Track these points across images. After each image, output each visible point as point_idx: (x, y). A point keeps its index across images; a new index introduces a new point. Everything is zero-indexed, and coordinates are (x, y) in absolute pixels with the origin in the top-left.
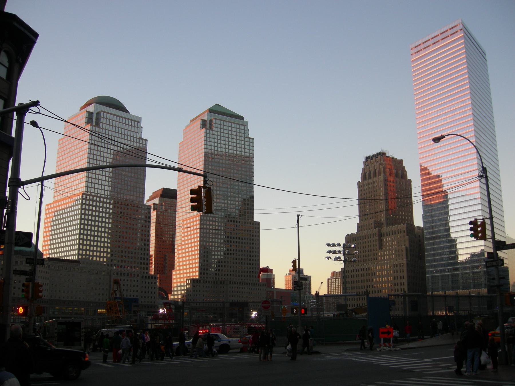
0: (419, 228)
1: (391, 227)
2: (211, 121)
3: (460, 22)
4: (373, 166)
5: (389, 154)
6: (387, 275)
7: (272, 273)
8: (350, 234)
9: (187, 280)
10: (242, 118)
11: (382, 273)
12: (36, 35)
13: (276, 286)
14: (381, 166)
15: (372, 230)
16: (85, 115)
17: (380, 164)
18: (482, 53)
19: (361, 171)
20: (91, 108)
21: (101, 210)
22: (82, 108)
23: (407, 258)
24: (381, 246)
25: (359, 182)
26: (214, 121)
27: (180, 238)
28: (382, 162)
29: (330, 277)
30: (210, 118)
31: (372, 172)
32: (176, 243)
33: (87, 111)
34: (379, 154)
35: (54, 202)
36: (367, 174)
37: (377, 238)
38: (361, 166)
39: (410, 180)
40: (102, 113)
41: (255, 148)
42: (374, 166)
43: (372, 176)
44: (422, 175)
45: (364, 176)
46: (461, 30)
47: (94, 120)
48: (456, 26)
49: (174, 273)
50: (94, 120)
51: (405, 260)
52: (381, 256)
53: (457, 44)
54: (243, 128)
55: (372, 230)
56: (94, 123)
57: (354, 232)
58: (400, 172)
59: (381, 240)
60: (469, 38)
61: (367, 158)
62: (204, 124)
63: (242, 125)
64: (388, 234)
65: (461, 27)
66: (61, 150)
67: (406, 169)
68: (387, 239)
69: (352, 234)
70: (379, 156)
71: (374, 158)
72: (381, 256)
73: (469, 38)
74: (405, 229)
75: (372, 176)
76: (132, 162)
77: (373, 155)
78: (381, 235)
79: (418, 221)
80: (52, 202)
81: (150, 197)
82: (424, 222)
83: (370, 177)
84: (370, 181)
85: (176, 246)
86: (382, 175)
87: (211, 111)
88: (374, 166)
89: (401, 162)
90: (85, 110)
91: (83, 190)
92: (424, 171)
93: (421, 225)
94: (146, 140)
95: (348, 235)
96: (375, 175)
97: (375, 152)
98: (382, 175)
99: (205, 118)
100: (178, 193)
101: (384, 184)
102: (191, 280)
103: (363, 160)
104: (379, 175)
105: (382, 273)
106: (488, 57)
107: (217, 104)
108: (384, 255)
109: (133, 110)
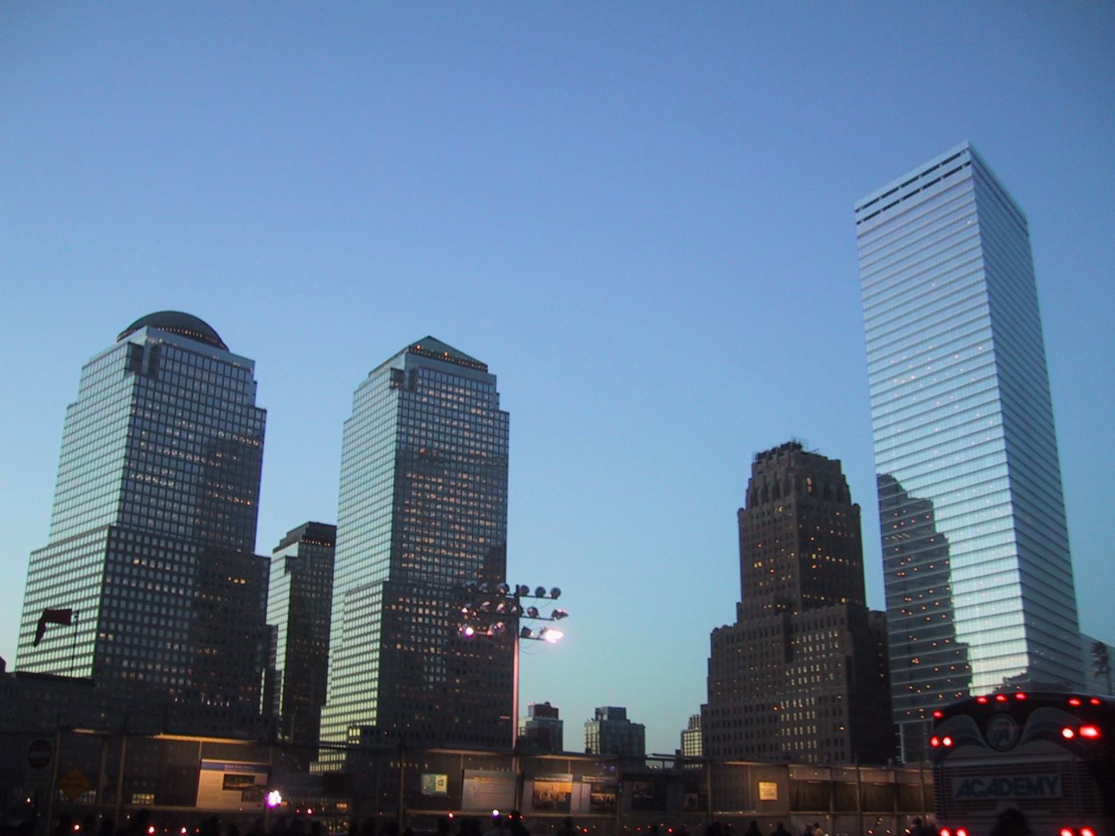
0: (878, 614)
1: (812, 610)
2: (413, 372)
3: (967, 146)
4: (772, 473)
5: (809, 448)
6: (805, 723)
7: (557, 716)
8: (720, 627)
9: (349, 728)
10: (483, 367)
11: (792, 717)
12: (254, 362)
13: (567, 747)
14: (791, 475)
15: (769, 618)
16: (124, 351)
17: (789, 469)
18: (1018, 222)
19: (746, 486)
20: (140, 338)
21: (152, 565)
22: (122, 336)
23: (849, 682)
24: (790, 655)
25: (741, 510)
26: (420, 372)
27: (340, 633)
28: (793, 464)
29: (686, 728)
30: (411, 366)
31: (770, 488)
32: (332, 644)
33: (129, 343)
34: (784, 447)
35: (50, 546)
36: (759, 492)
37: (781, 636)
38: (745, 474)
39: (856, 505)
40: (164, 348)
41: (511, 435)
42: (775, 475)
43: (770, 495)
44: (881, 492)
45: (754, 495)
46: (968, 164)
47: (145, 363)
48: (958, 155)
49: (324, 712)
50: (145, 363)
51: (844, 686)
52: (810, 708)
53: (961, 198)
54: (486, 388)
55: (769, 618)
56: (145, 370)
57: (730, 624)
58: (833, 488)
59: (788, 640)
60: (989, 189)
61: (760, 456)
62: (397, 376)
63: (483, 383)
64: (807, 628)
65: (966, 158)
66: (71, 430)
67: (848, 481)
68: (806, 642)
69: (725, 627)
70: (786, 452)
71: (775, 456)
72: (810, 708)
73: (989, 189)
74: (844, 616)
75: (770, 495)
76: (235, 463)
77: (774, 450)
78: (790, 630)
79: (875, 599)
80: (46, 545)
81: (281, 541)
82: (889, 601)
83: (765, 499)
84: (766, 507)
85: (331, 652)
86: (793, 493)
87: (412, 351)
88: (775, 475)
89: (837, 464)
90: (126, 340)
91: (112, 519)
92: (888, 487)
93: (882, 607)
94: (265, 411)
95: (716, 629)
96: (777, 495)
97: (777, 443)
98: (793, 493)
99: (401, 365)
100: (339, 532)
101: (799, 515)
102: (362, 728)
103: (750, 460)
104: (787, 493)
105: (792, 717)
106: (1031, 228)
107: (429, 337)
108: (796, 676)
109: (237, 345)
